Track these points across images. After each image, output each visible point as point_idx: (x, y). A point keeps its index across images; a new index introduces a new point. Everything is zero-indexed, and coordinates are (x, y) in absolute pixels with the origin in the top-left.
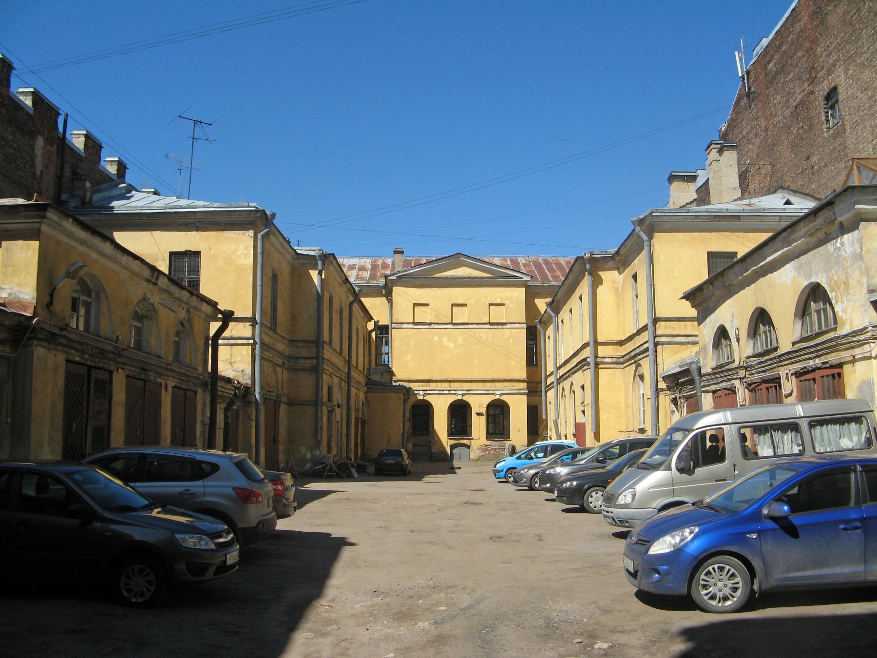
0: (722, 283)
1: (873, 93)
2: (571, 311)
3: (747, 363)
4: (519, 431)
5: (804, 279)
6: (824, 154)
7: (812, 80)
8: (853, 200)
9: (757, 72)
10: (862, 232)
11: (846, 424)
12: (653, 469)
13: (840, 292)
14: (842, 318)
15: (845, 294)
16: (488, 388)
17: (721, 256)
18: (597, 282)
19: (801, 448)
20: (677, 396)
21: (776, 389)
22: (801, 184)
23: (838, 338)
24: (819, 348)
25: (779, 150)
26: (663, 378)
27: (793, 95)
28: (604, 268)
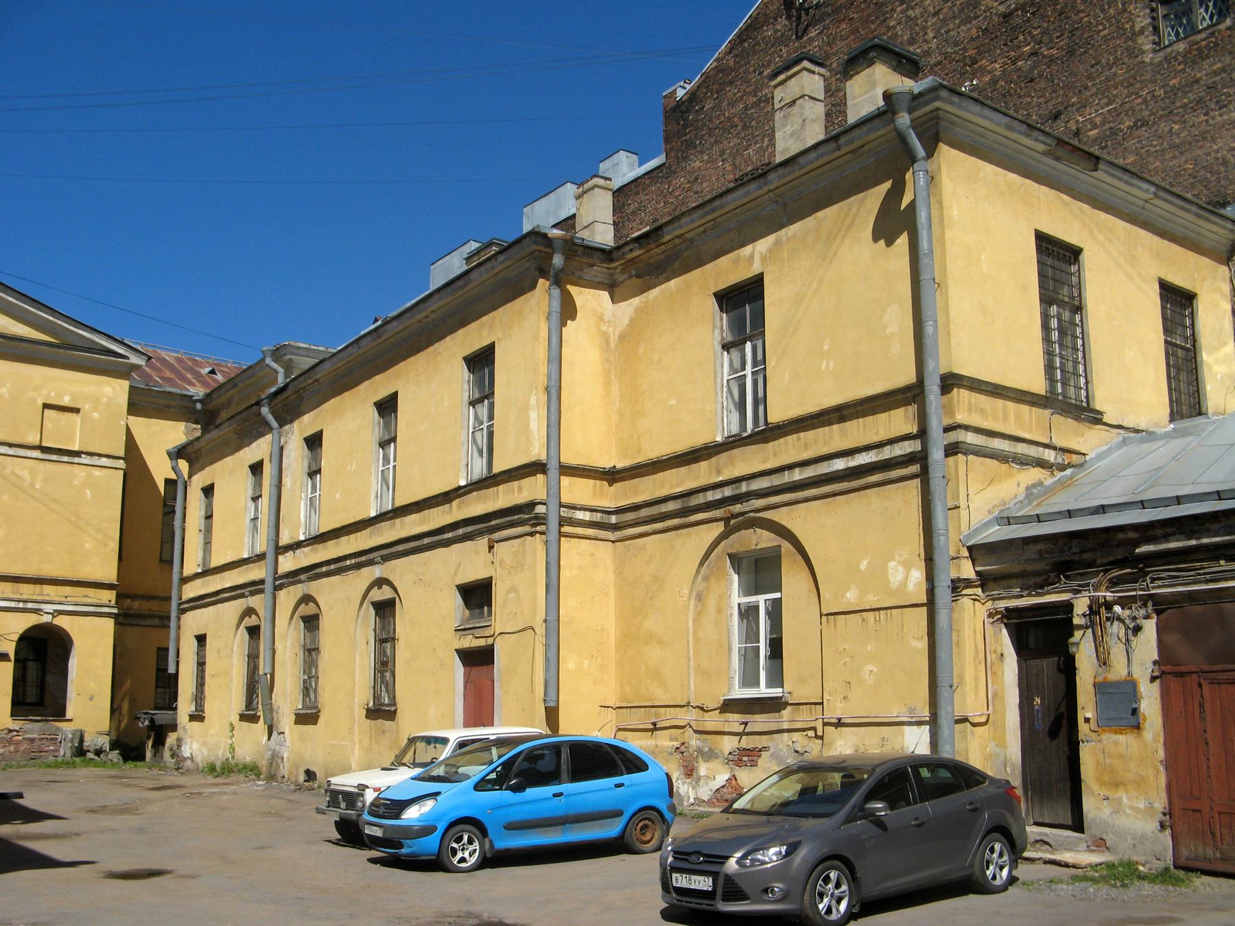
4: (91, 698)
16: (25, 597)
28: (581, 278)
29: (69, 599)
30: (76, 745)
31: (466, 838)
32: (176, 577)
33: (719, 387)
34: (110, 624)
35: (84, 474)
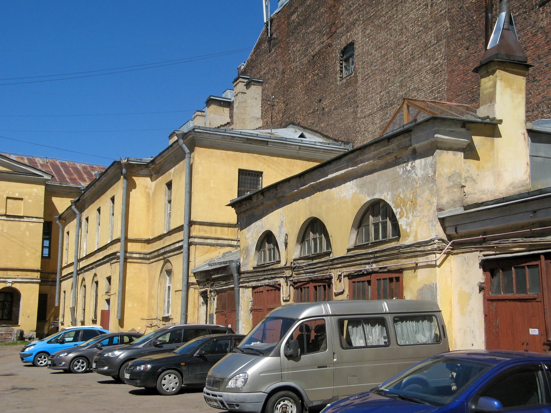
0: (273, 195)
1: (386, 52)
2: (99, 210)
3: (294, 264)
4: (29, 317)
5: (366, 195)
6: (336, 99)
7: (331, 35)
8: (434, 130)
9: (280, 21)
10: (437, 158)
11: (421, 321)
12: (262, 355)
13: (406, 209)
14: (406, 230)
15: (411, 210)
17: (252, 174)
18: (131, 186)
19: (386, 340)
20: (207, 290)
21: (325, 289)
22: (311, 123)
23: (400, 247)
24: (378, 255)
25: (294, 91)
26: (194, 273)
27: (312, 45)
28: (138, 174)
29: (19, 277)
30: (19, 336)
31: (43, 357)
32: (59, 268)
33: (166, 215)
34: (37, 286)
35: (25, 225)
